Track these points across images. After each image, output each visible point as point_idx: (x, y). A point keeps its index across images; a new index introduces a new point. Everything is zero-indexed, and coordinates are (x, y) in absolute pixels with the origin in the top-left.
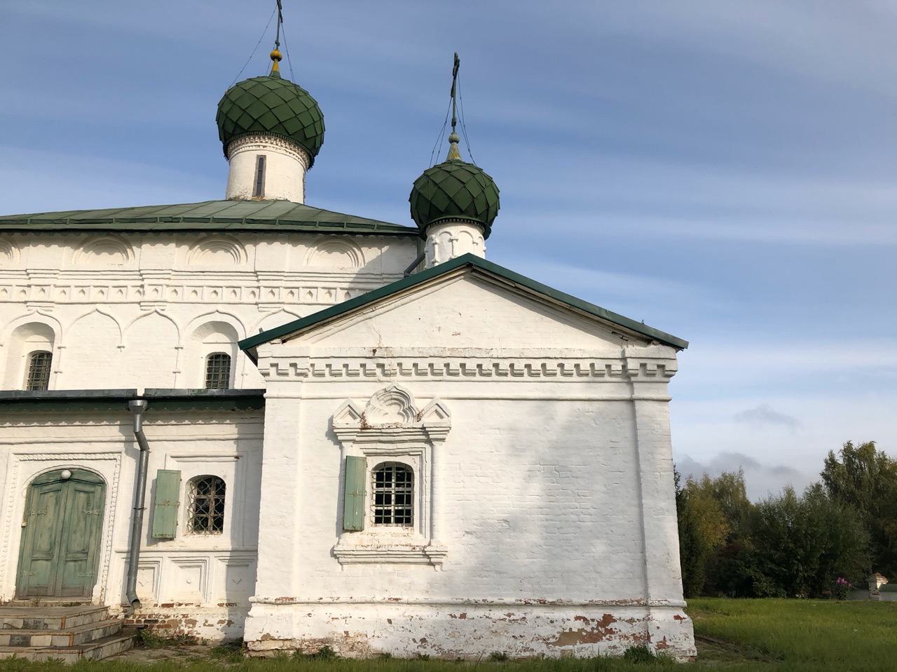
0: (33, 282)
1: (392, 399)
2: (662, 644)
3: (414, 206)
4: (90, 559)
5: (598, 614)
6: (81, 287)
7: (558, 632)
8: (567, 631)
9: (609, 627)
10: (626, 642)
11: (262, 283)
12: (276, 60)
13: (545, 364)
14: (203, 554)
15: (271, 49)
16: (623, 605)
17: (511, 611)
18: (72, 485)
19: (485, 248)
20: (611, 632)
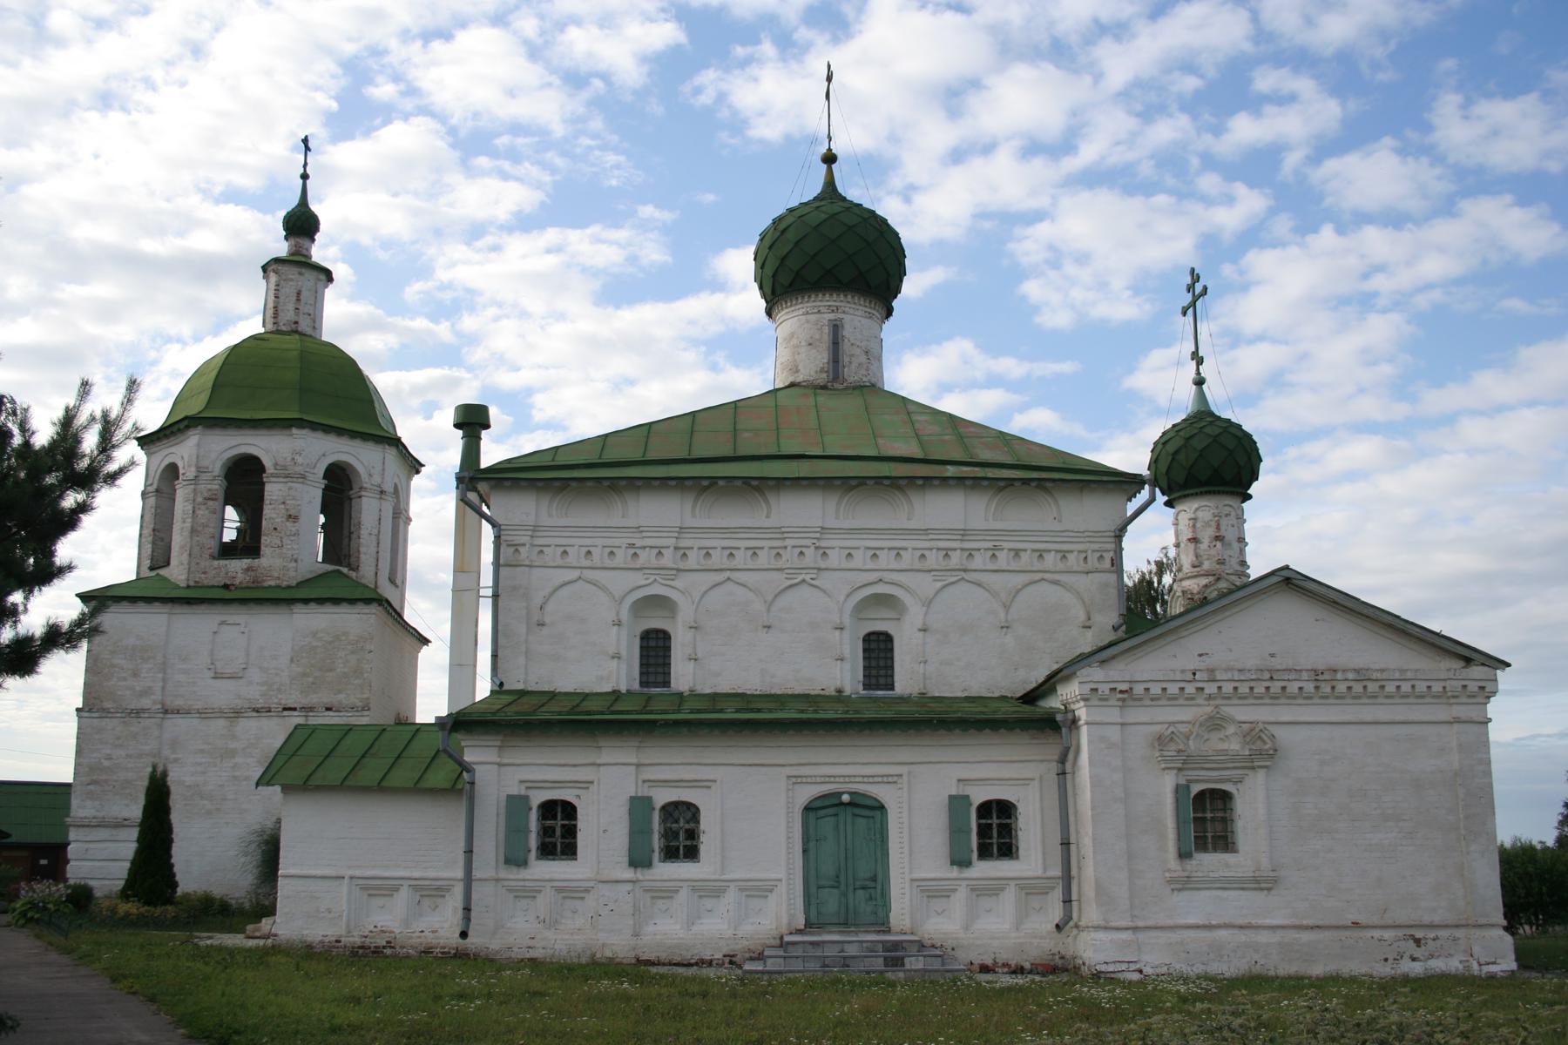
1: (1214, 725)
3: (1153, 460)
4: (879, 887)
6: (587, 546)
13: (1148, 689)
14: (1003, 882)
18: (850, 810)
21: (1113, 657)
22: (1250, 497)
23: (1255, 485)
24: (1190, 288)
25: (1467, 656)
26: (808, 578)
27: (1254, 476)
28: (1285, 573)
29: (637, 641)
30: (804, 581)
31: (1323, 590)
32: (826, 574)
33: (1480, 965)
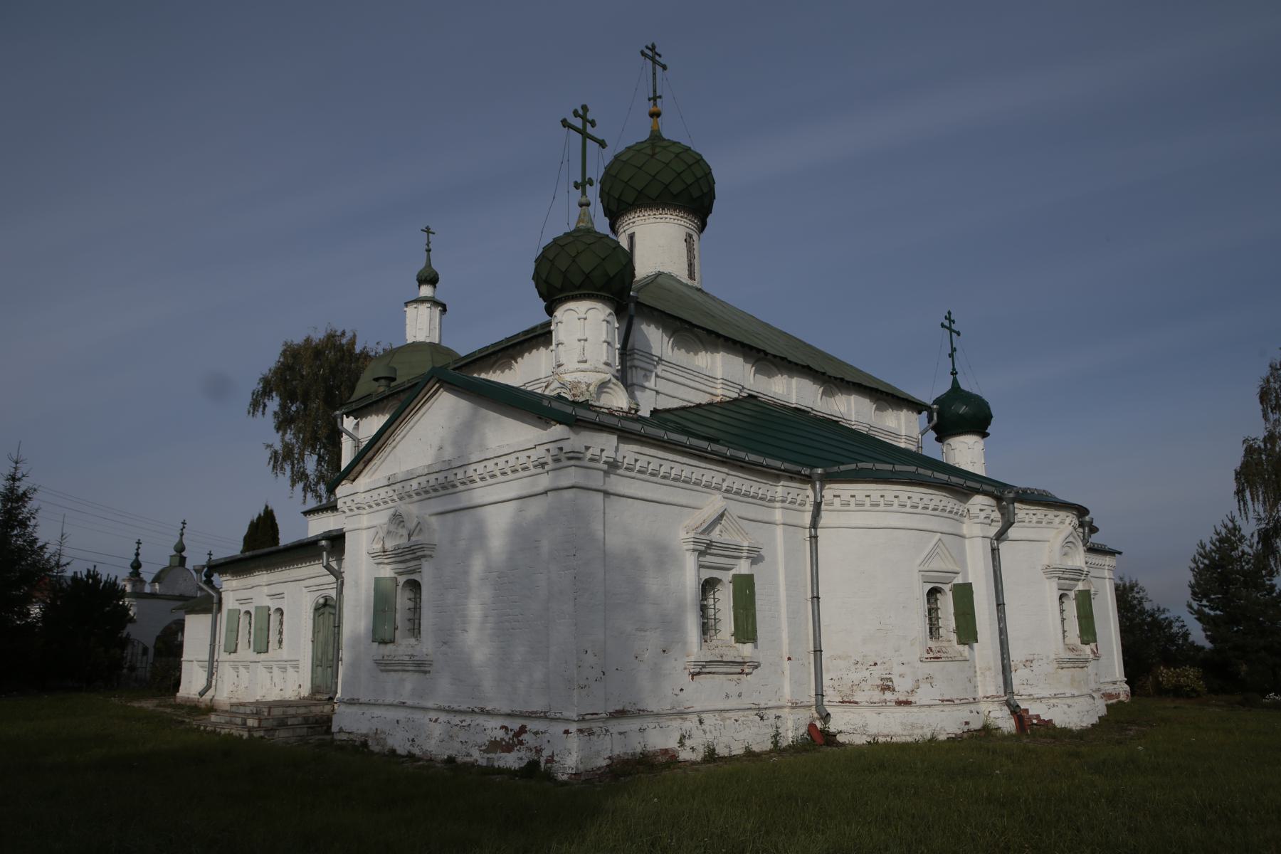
2: (550, 760)
5: (515, 725)
7: (488, 741)
8: (493, 739)
9: (520, 738)
10: (529, 754)
12: (655, 118)
15: (649, 107)
16: (533, 715)
17: (463, 718)
20: (521, 743)
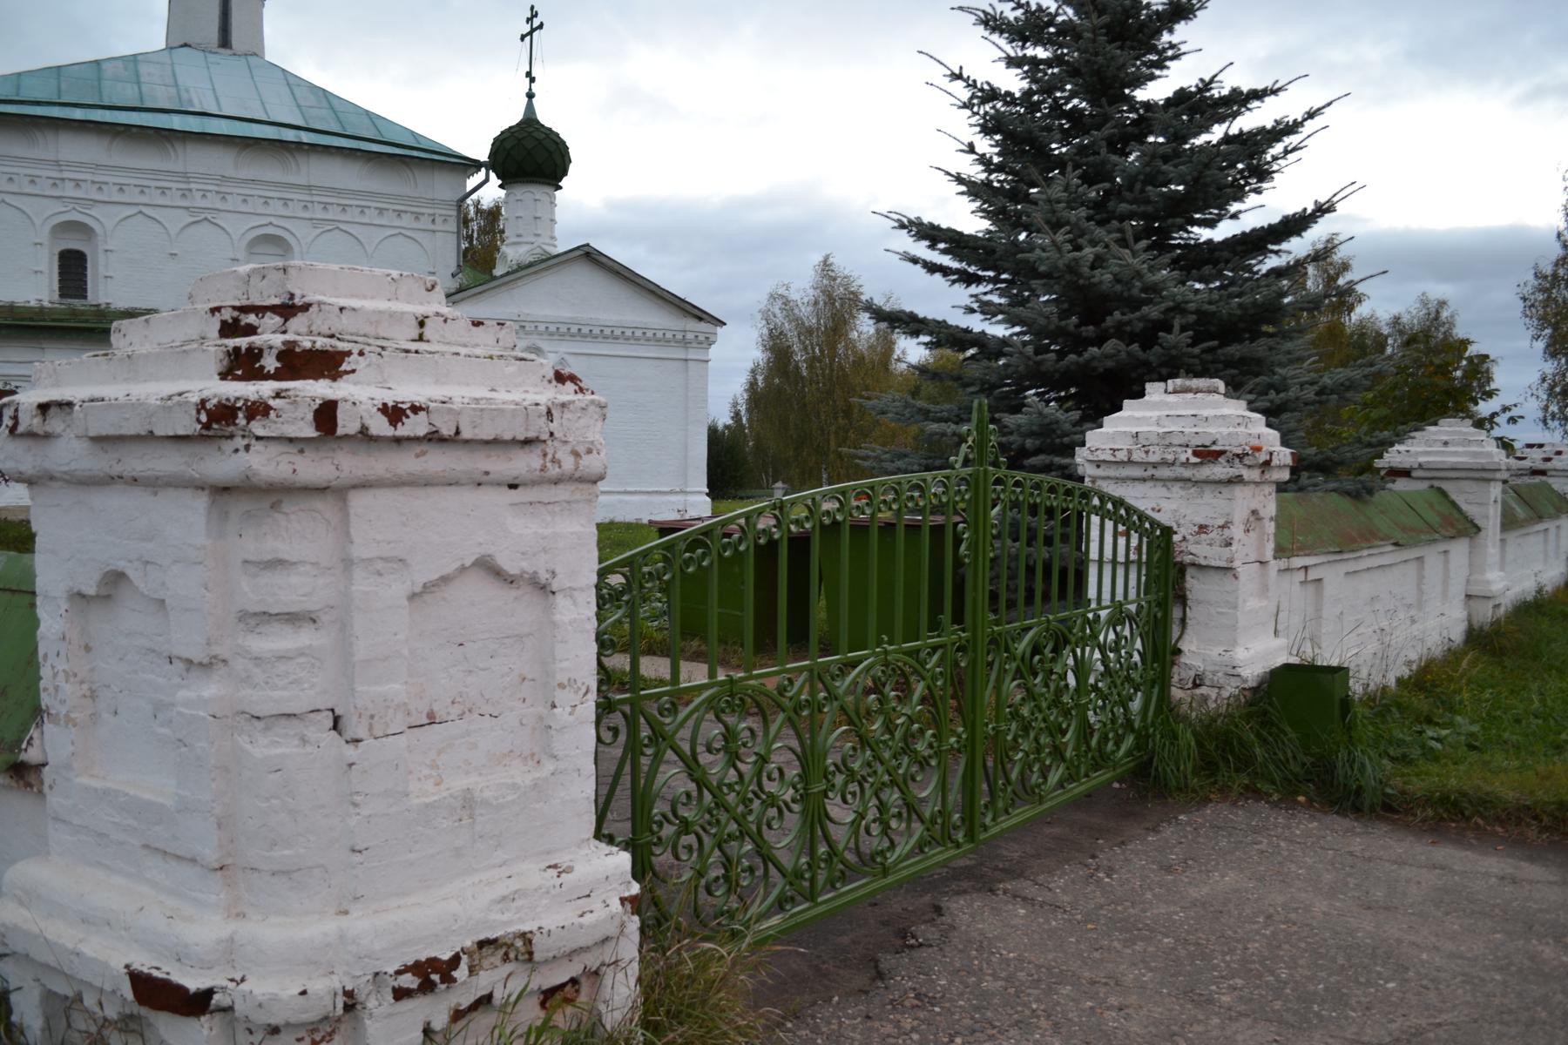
0: (66, 175)
11: (193, 186)
19: (500, 182)
21: (462, 300)
22: (561, 188)
23: (565, 179)
24: (529, 20)
25: (700, 315)
26: (209, 217)
27: (565, 173)
28: (586, 249)
29: (56, 258)
30: (206, 219)
31: (611, 263)
32: (222, 214)
33: (576, 454)
